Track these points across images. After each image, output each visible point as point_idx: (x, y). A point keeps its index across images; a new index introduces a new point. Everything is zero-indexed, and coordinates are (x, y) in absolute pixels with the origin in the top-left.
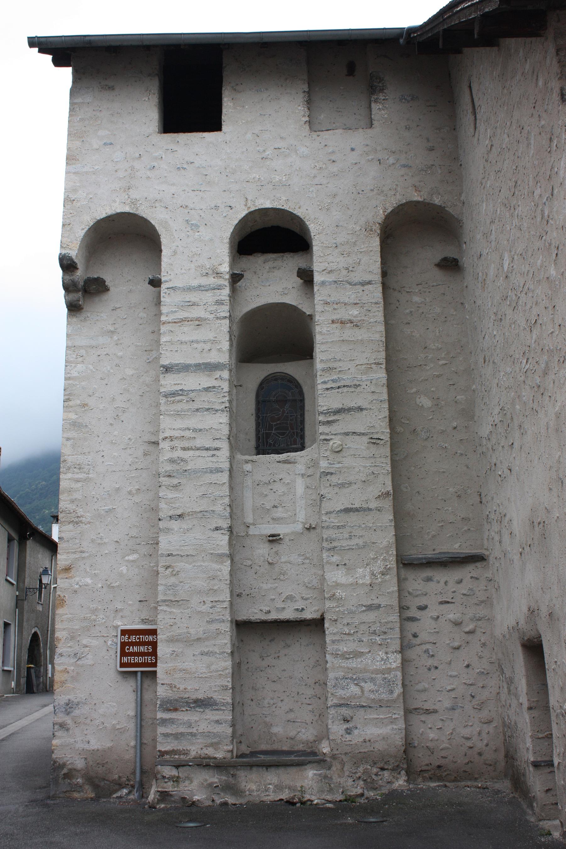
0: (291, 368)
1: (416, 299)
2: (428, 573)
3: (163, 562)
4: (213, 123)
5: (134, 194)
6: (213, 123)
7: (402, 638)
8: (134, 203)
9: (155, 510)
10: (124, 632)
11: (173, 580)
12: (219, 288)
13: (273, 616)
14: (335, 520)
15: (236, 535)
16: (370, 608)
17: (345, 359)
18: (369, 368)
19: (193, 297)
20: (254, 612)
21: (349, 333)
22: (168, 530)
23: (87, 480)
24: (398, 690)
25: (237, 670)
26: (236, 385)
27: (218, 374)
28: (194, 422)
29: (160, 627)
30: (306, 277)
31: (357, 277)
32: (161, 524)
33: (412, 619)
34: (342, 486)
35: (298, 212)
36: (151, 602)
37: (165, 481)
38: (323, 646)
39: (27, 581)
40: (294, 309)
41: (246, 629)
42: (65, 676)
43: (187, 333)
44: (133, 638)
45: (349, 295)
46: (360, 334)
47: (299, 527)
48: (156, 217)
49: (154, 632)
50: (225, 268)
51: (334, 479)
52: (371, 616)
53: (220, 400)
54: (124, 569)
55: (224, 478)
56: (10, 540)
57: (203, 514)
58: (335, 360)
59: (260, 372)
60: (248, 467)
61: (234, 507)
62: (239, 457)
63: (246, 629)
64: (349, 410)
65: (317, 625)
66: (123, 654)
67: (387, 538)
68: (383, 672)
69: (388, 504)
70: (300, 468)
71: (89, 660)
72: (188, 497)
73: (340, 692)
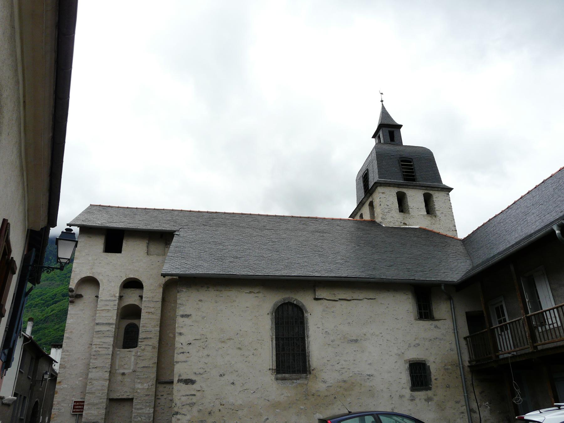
0: (135, 322)
1: (172, 305)
2: (165, 385)
3: (89, 381)
4: (119, 250)
5: (93, 271)
6: (119, 250)
7: (155, 404)
8: (93, 273)
9: (89, 365)
10: (75, 402)
11: (91, 386)
12: (115, 301)
13: (120, 397)
14: (140, 370)
15: (112, 373)
16: (147, 395)
17: (148, 324)
18: (155, 327)
19: (107, 303)
20: (115, 396)
21: (151, 316)
22: (91, 372)
23: (69, 355)
24: (152, 419)
25: (107, 414)
26: (118, 328)
27: (112, 326)
28: (103, 340)
29: (85, 400)
30: (141, 297)
31: (155, 300)
32: (90, 370)
33: (159, 399)
34: (143, 360)
35: (141, 279)
36: (84, 393)
37: (92, 357)
38: (132, 406)
39: (37, 376)
40: (137, 306)
41: (112, 401)
42: (55, 416)
43: (104, 314)
44: (77, 404)
45: (152, 305)
46: (154, 317)
47: (131, 371)
48: (99, 278)
49: (83, 402)
50: (118, 295)
51: (141, 358)
52: (147, 398)
53: (112, 334)
54: (77, 382)
55: (110, 357)
56: (32, 359)
57: (102, 367)
58: (146, 323)
59: (127, 322)
60: (118, 352)
61: (112, 365)
62: (117, 349)
63: (112, 401)
64: (148, 338)
65: (132, 400)
66: (74, 408)
67: (154, 376)
68: (148, 414)
69: (155, 366)
70: (133, 353)
71: (63, 410)
72: (98, 362)
73: (135, 420)
